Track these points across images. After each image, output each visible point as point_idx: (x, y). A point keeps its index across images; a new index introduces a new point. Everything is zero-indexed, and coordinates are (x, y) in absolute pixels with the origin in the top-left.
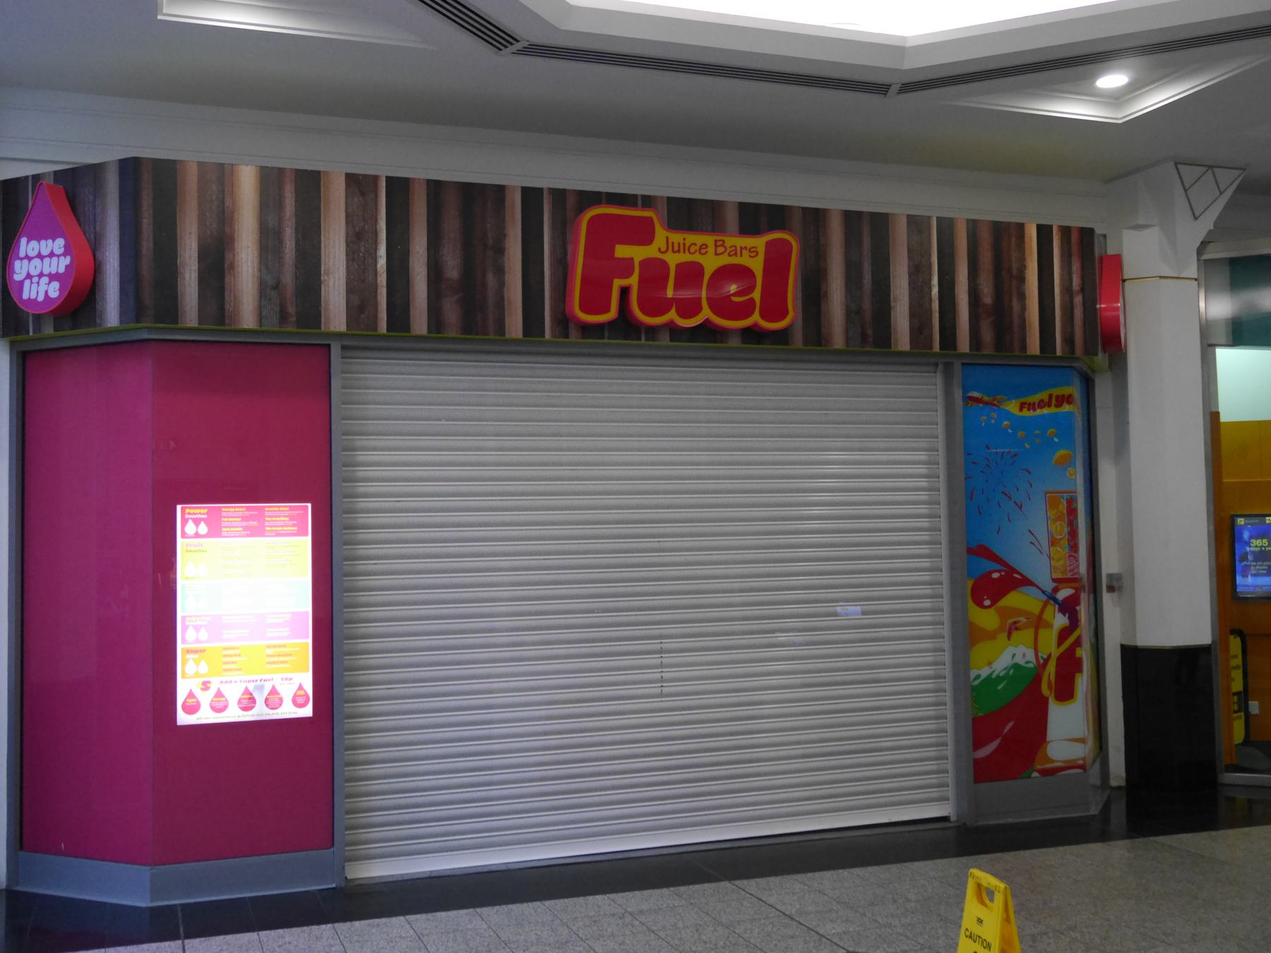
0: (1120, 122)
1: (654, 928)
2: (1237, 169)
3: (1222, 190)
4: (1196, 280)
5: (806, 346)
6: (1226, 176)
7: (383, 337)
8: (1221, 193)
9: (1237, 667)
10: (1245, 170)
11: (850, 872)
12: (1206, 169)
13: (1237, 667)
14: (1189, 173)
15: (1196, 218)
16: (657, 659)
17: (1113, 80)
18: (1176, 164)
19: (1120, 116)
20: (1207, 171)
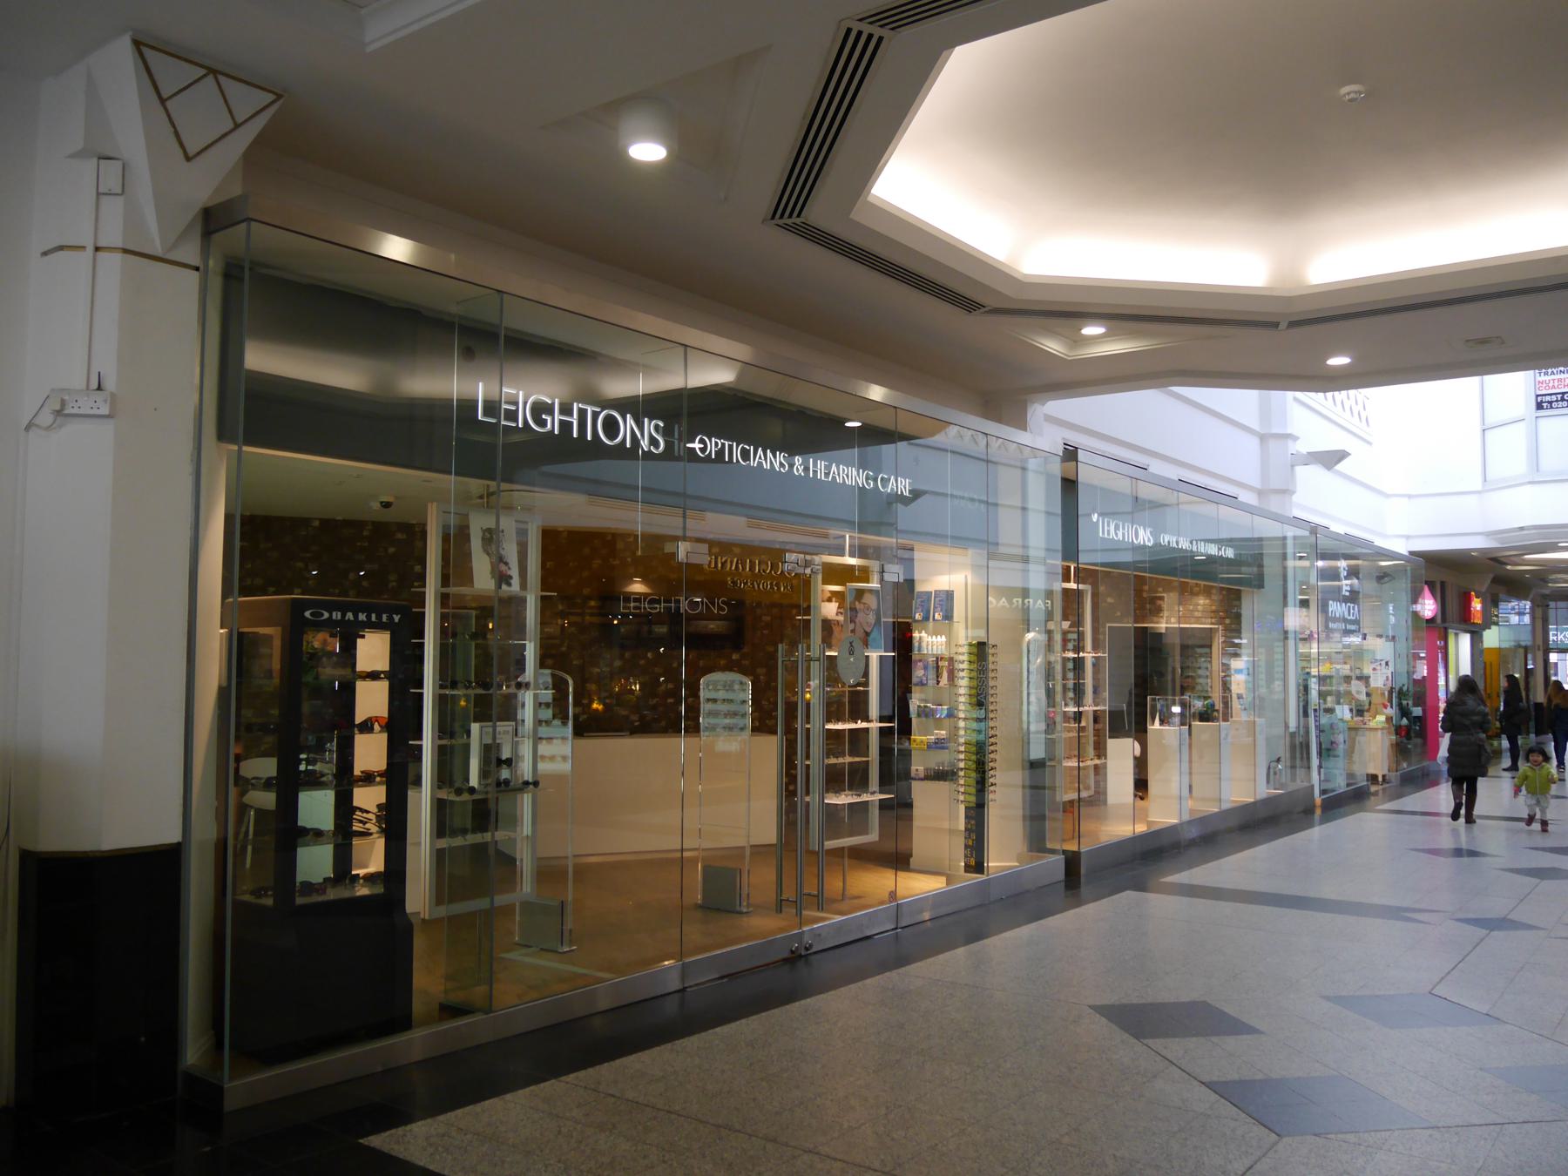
0: (1070, 358)
1: (806, 1157)
2: (201, 66)
3: (239, 121)
4: (197, 269)
5: (242, 524)
6: (246, 100)
7: (824, 727)
8: (237, 126)
9: (368, 778)
10: (279, 97)
11: (899, 974)
12: (203, 72)
13: (368, 778)
14: (172, 74)
15: (188, 159)
16: (691, 984)
17: (1091, 330)
18: (137, 44)
19: (1071, 354)
20: (205, 76)
